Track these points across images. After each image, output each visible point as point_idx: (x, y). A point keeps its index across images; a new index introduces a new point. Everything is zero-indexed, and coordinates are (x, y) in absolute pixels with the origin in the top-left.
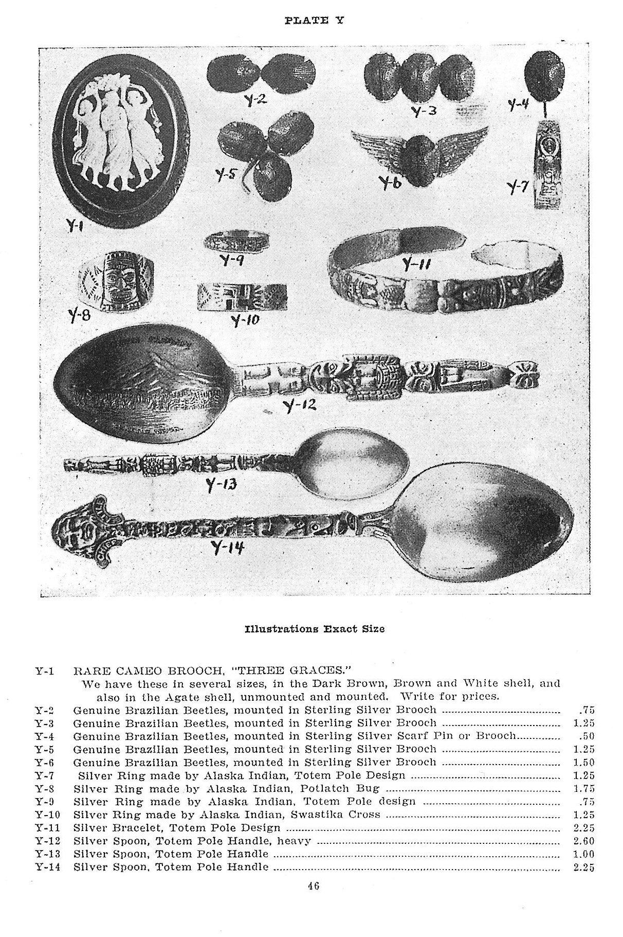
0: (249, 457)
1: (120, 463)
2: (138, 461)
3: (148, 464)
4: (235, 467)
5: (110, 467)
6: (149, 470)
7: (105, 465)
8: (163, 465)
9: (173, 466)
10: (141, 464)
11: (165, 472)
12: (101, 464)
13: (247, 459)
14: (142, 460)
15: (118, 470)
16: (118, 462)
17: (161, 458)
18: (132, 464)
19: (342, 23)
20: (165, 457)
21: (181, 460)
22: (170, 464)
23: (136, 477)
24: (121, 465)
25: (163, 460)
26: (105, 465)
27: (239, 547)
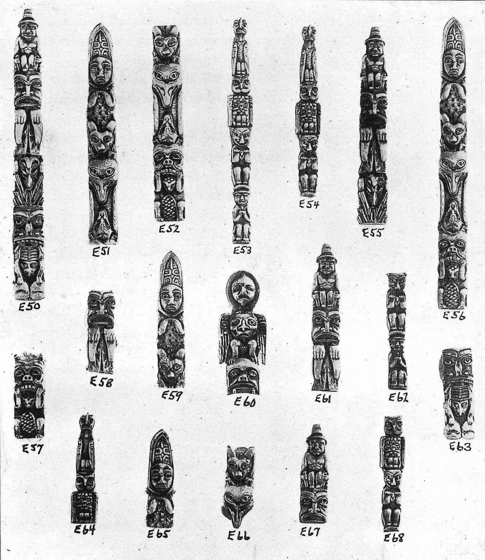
0: (246, 198)
1: (242, 73)
2: (244, 91)
3: (241, 100)
4: (237, 184)
5: (307, 70)
6: (235, 101)
7: (241, 58)
8: (240, 115)
9: (307, 131)
10: (242, 94)
11: (234, 117)
12: (310, 62)
13: (244, 196)
14: (246, 94)
15: (236, 71)
16: (243, 71)
17: (247, 113)
18: (242, 84)
19: (179, 232)
20: (248, 117)
21: (245, 132)
22: (241, 121)
23: (228, 90)
24: (309, 81)
25: (313, 122)
26: (241, 58)
27: (316, 204)
